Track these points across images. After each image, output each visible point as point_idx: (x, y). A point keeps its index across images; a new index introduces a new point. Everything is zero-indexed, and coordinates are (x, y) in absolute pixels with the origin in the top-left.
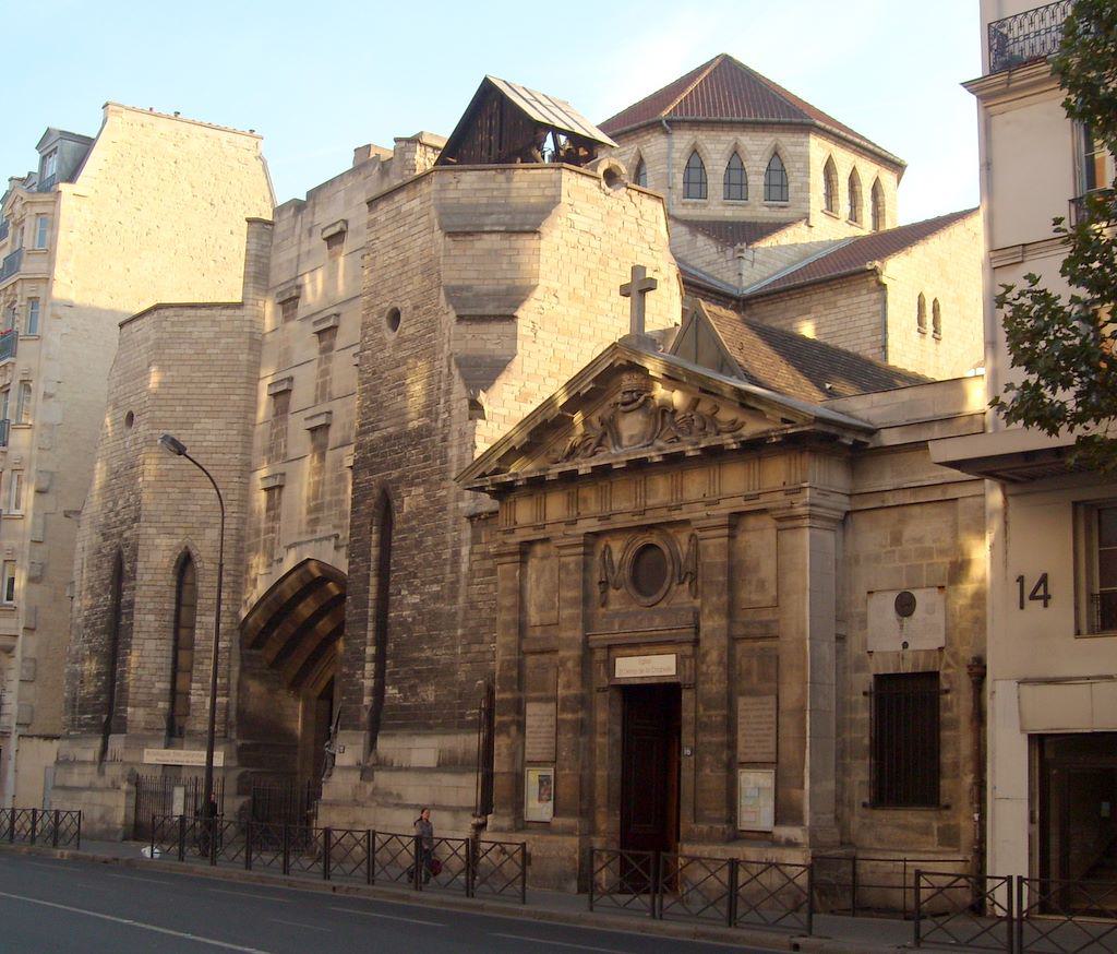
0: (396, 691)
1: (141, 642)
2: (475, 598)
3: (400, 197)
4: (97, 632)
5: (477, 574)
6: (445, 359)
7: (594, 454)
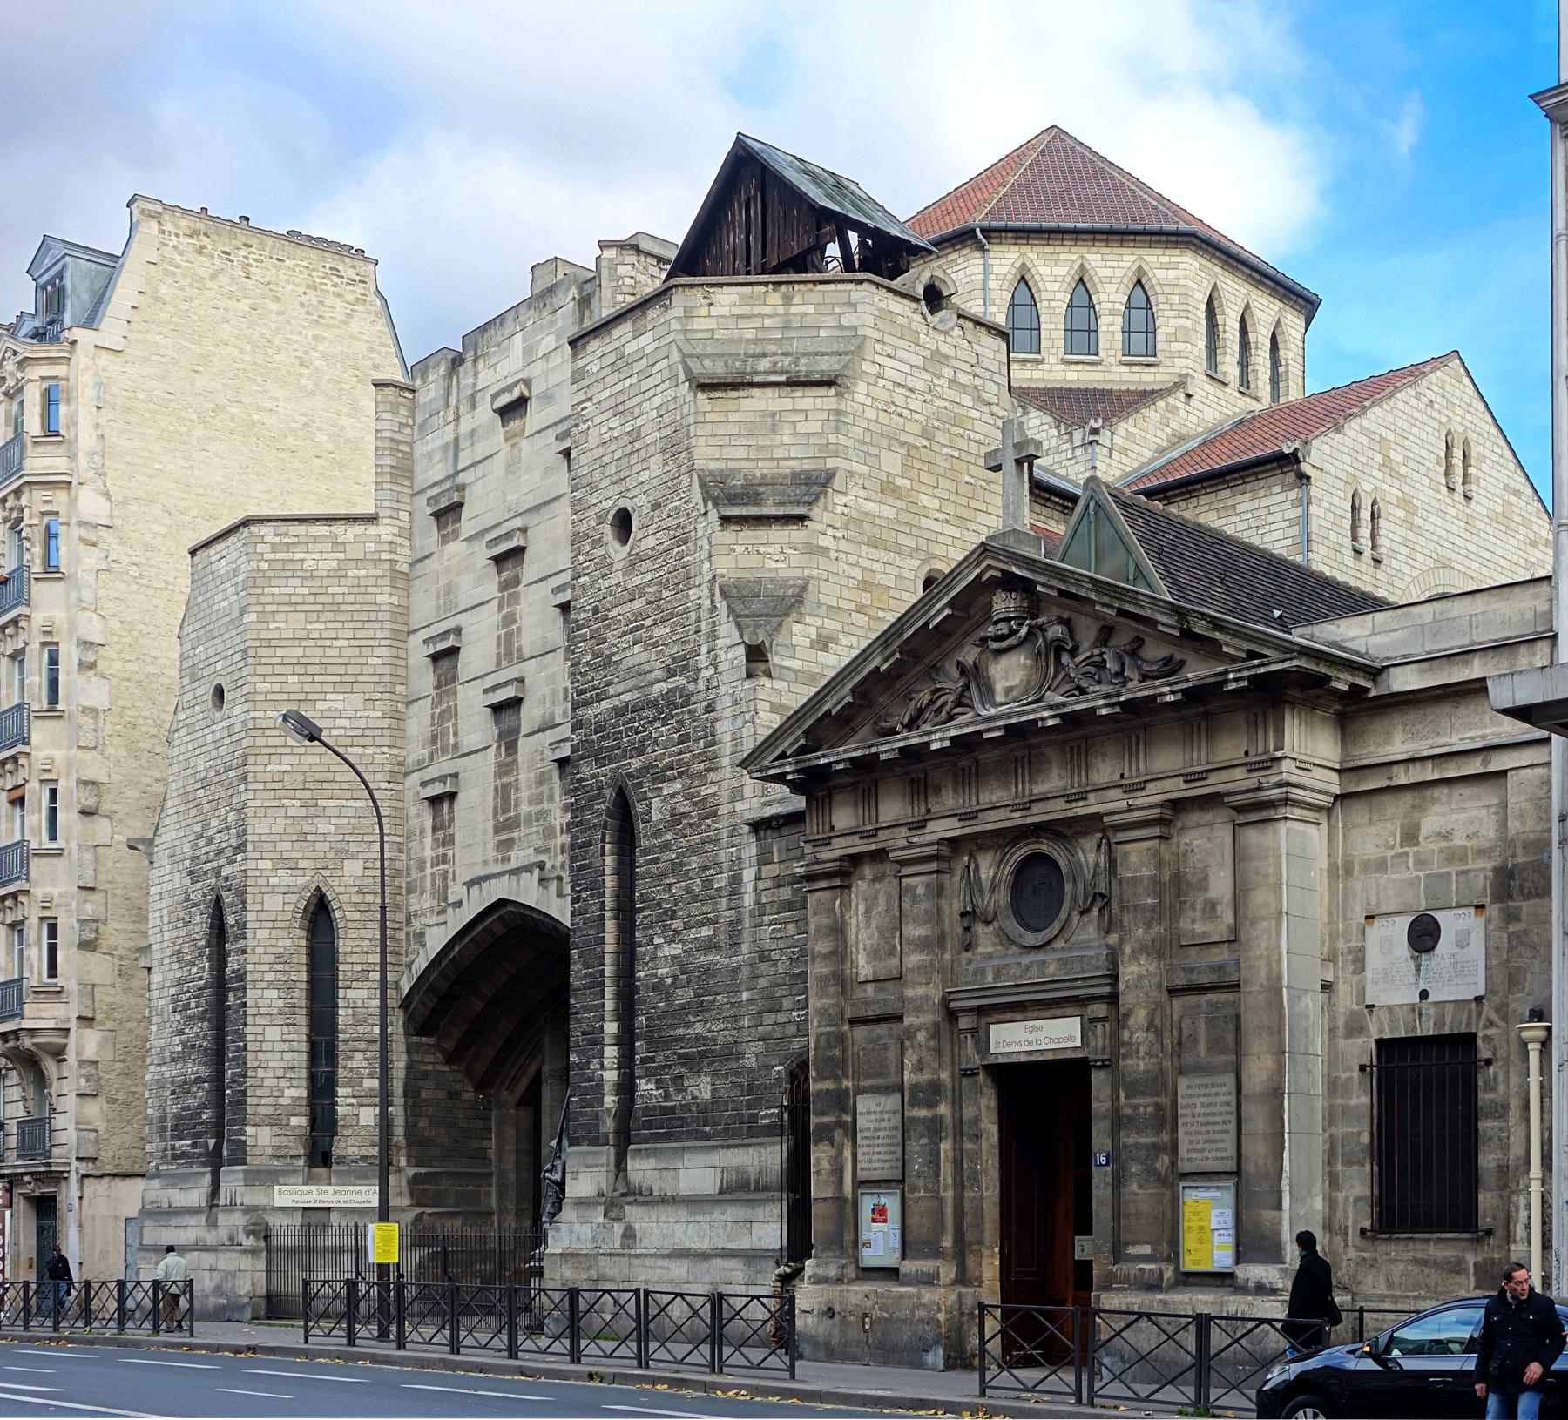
0: (653, 1086)
1: (259, 1030)
2: (767, 944)
3: (623, 330)
4: (191, 1018)
5: (768, 910)
6: (705, 587)
7: (951, 718)
